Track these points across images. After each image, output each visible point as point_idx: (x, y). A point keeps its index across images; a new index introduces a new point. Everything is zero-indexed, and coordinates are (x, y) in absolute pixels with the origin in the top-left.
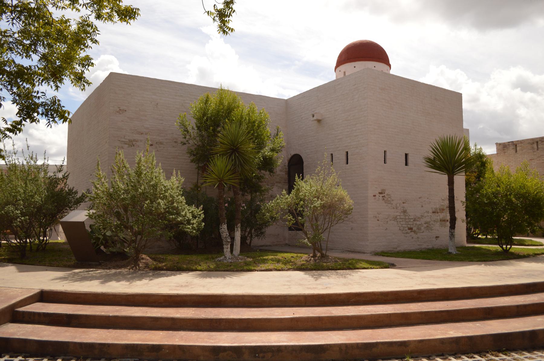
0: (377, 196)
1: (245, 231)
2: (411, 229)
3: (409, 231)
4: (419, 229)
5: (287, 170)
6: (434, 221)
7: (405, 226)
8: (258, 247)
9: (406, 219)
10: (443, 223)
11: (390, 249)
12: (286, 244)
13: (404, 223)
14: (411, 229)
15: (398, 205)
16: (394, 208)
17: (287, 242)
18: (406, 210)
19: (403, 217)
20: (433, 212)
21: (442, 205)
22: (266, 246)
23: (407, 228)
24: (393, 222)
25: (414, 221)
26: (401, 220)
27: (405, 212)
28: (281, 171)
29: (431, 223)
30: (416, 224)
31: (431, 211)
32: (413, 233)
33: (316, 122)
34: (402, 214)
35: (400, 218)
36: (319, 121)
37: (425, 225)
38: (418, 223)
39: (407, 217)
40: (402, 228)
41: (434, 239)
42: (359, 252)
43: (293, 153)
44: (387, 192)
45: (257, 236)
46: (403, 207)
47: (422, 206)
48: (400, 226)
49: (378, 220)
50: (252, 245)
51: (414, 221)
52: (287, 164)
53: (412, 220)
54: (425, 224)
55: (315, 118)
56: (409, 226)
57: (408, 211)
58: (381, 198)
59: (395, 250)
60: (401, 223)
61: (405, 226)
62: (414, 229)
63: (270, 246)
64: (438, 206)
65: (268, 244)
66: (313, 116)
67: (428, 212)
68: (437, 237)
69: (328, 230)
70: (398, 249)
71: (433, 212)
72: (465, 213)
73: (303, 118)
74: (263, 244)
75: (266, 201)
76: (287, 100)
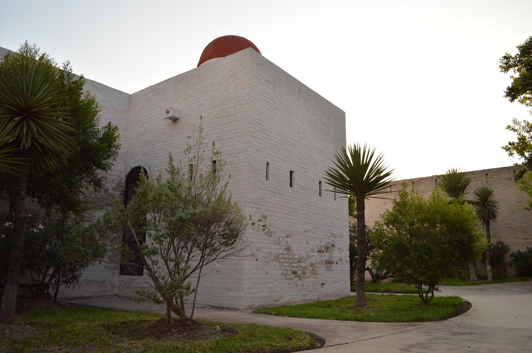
0: (256, 224)
1: (362, 270)
2: (295, 273)
3: (294, 276)
4: (304, 273)
5: (124, 189)
6: (320, 263)
7: (289, 268)
8: (71, 300)
9: (289, 259)
10: (329, 265)
11: (270, 302)
12: (115, 295)
13: (287, 265)
14: (295, 273)
15: (281, 239)
16: (276, 243)
17: (116, 291)
18: (290, 247)
19: (286, 256)
20: (319, 251)
21: (327, 243)
22: (84, 298)
23: (290, 272)
24: (275, 263)
25: (299, 262)
26: (284, 260)
27: (288, 249)
28: (114, 189)
29: (316, 265)
30: (301, 266)
31: (316, 250)
32: (297, 278)
33: (171, 121)
34: (285, 252)
35: (283, 258)
36: (175, 120)
37: (310, 268)
38: (303, 265)
39: (291, 257)
40: (285, 272)
41: (319, 287)
42: (228, 309)
43: (133, 165)
44: (268, 220)
45: (66, 282)
46: (287, 243)
47: (307, 243)
48: (283, 268)
49: (257, 260)
50: (59, 296)
51: (299, 262)
52: (124, 181)
53: (296, 261)
54: (311, 266)
55: (170, 115)
56: (293, 269)
57: (292, 248)
58: (261, 227)
59: (276, 303)
60: (285, 264)
61: (289, 268)
62: (299, 273)
63: (89, 297)
64: (323, 244)
65: (87, 294)
66: (168, 112)
67: (313, 251)
68: (323, 284)
69: (198, 271)
70: (281, 302)
71: (319, 251)
72: (348, 253)
73: (152, 118)
74: (75, 295)
75: (161, 285)
76: (131, 95)
